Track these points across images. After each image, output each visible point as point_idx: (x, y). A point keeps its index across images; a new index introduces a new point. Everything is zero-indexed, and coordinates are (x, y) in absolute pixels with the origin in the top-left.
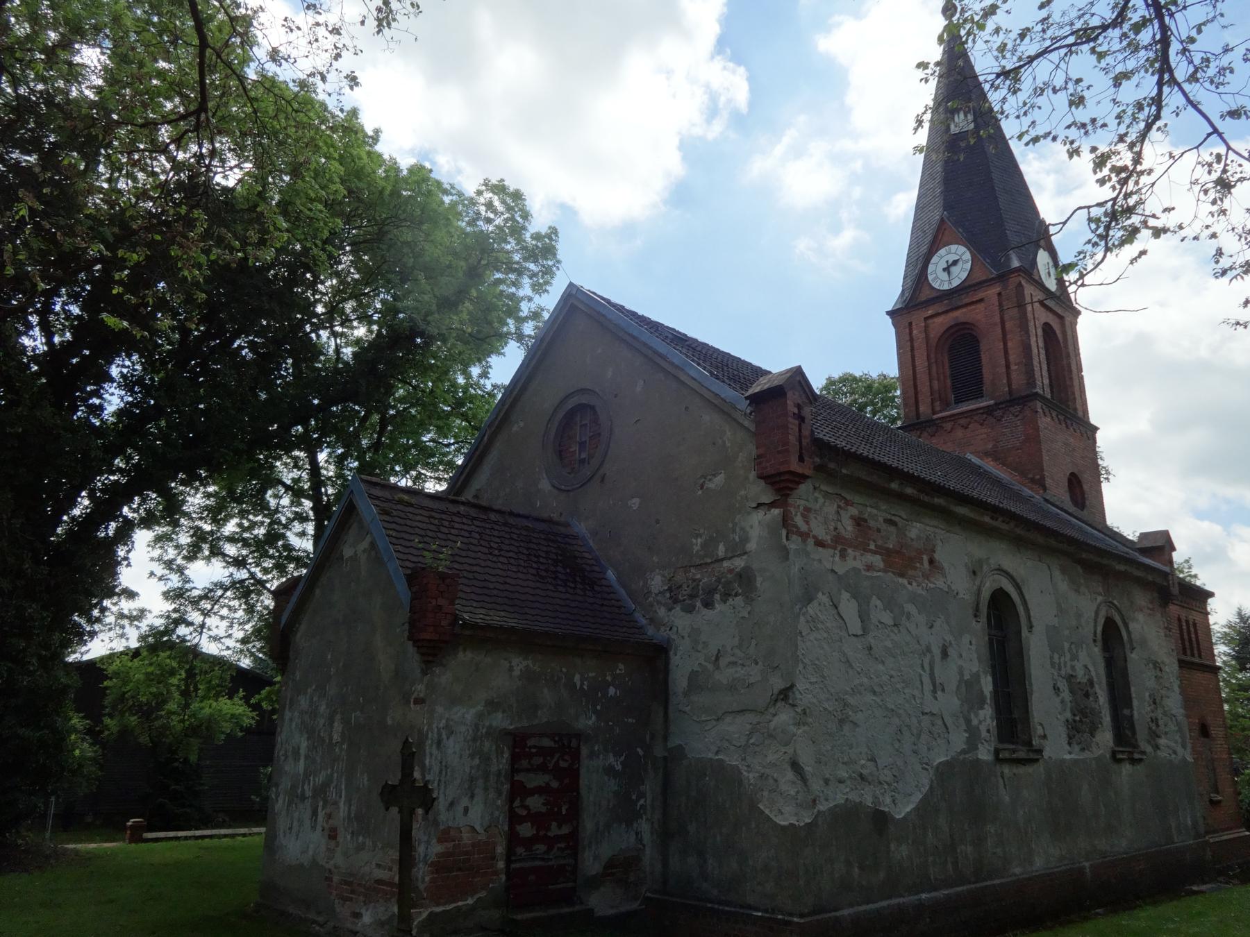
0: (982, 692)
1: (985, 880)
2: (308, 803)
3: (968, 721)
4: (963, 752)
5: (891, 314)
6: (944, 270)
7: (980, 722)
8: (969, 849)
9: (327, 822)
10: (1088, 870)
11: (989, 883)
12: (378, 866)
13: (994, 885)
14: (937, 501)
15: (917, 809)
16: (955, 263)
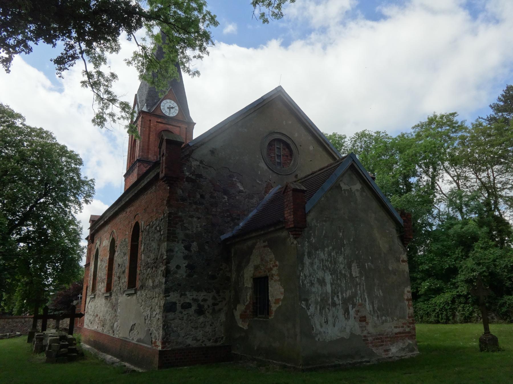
2: (340, 307)
5: (195, 124)
6: (168, 108)
9: (357, 314)
12: (396, 327)
16: (172, 108)
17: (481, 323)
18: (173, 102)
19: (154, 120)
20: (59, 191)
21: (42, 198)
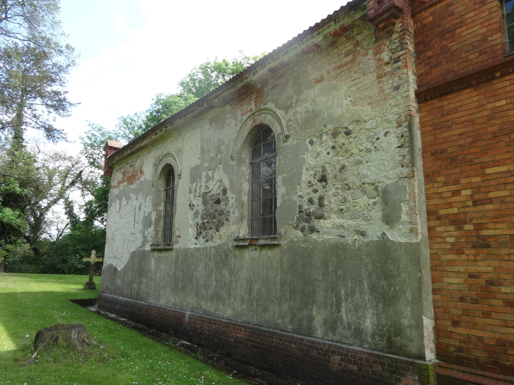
0: (151, 219)
1: (138, 300)
3: (144, 234)
4: (140, 247)
7: (148, 234)
8: (136, 286)
10: (187, 316)
11: (138, 302)
13: (139, 304)
14: (138, 146)
15: (124, 268)
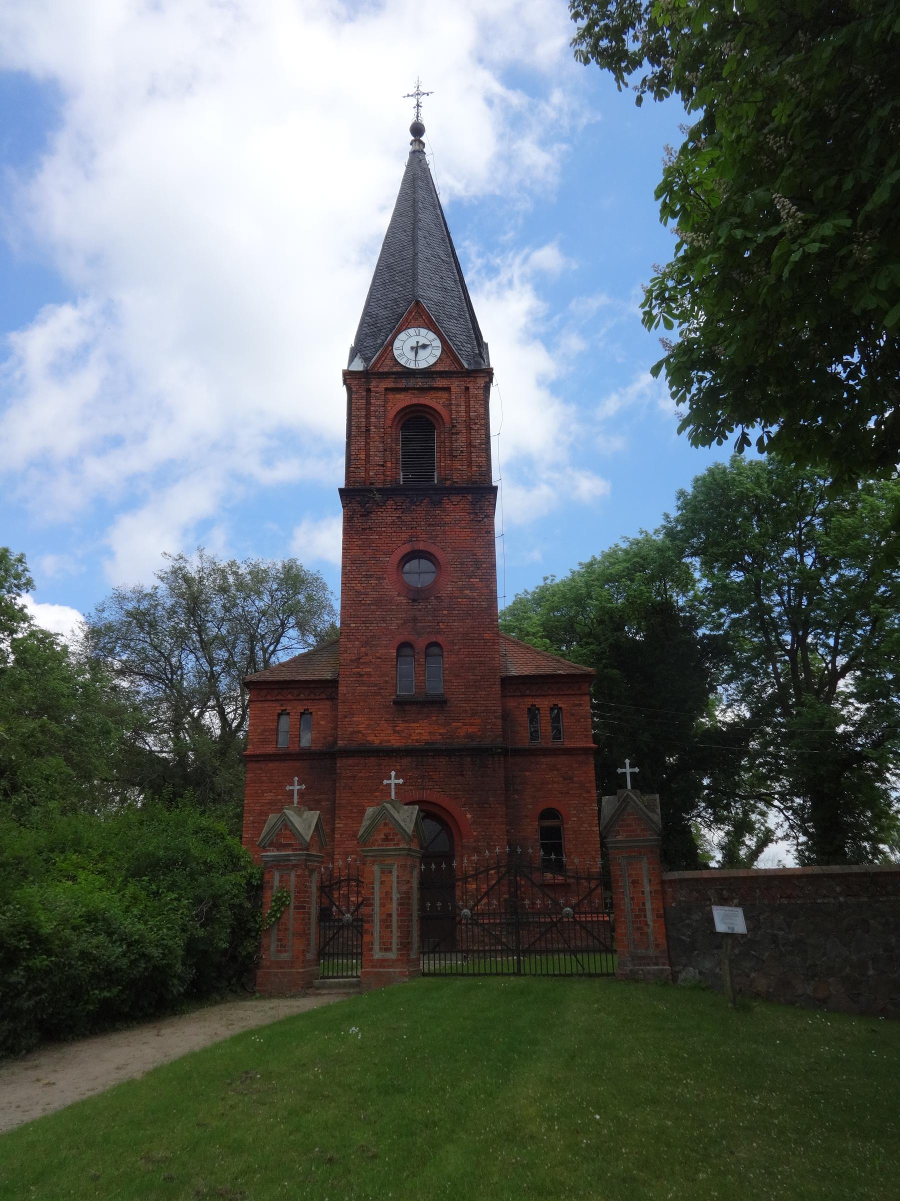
6: (412, 348)
16: (424, 346)
17: (507, 158)
18: (424, 331)
19: (379, 386)
20: (799, 90)
21: (362, 1037)
